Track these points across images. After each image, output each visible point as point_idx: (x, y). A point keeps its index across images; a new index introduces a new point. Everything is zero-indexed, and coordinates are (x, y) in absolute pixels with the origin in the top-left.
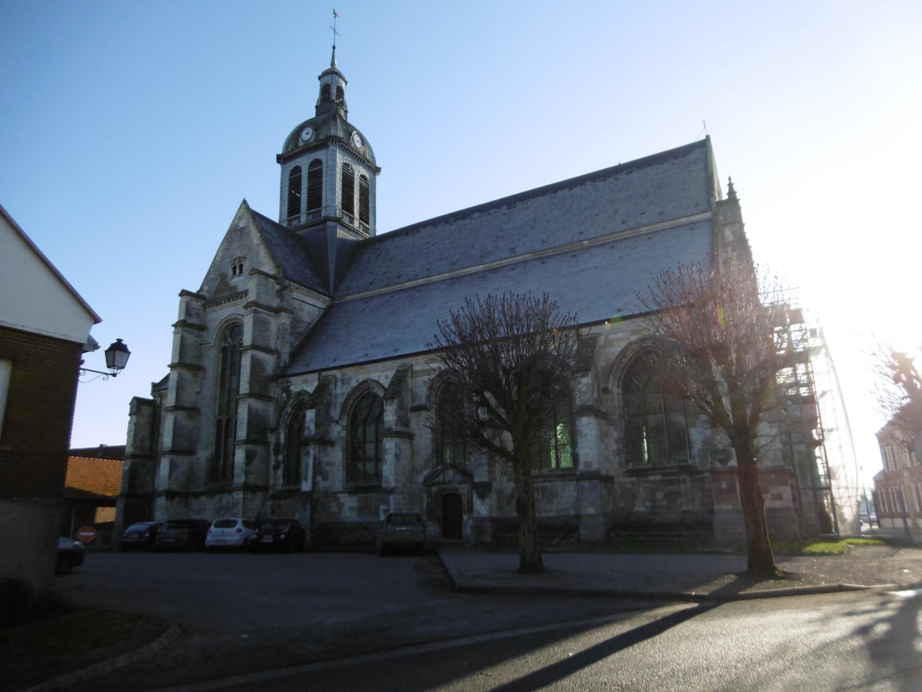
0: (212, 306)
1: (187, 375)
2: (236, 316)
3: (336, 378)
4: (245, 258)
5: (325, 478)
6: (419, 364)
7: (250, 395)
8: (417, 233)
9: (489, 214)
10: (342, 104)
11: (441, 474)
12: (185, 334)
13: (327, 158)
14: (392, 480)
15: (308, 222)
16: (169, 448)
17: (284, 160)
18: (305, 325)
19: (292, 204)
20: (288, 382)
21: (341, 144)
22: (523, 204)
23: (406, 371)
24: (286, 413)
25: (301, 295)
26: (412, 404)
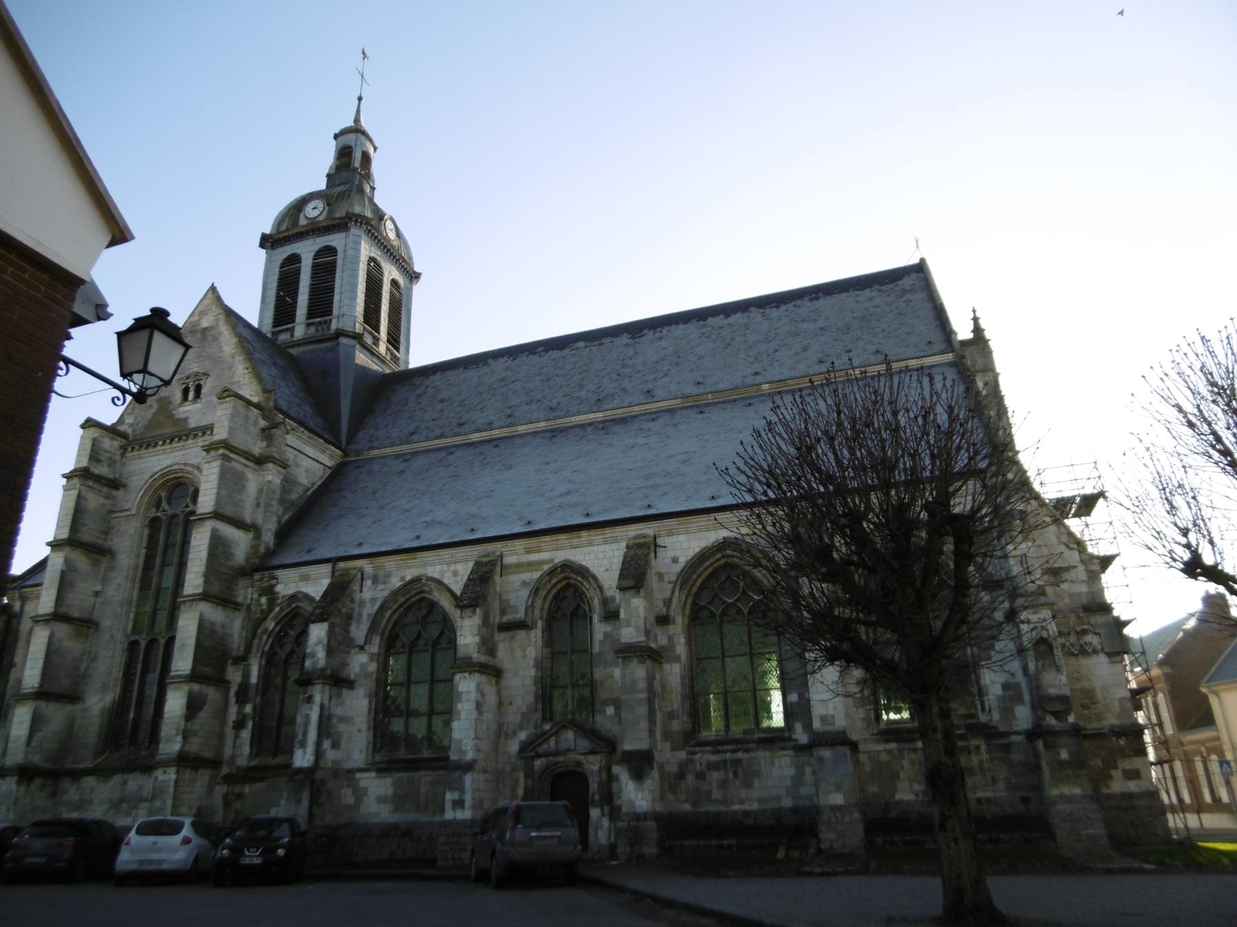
0: (139, 450)
1: (81, 561)
2: (183, 467)
3: (363, 574)
4: (207, 375)
5: (336, 745)
6: (514, 554)
7: (205, 597)
8: (484, 365)
9: (601, 344)
10: (368, 176)
11: (553, 738)
12: (85, 491)
13: (346, 245)
14: (469, 748)
15: (306, 337)
16: (33, 687)
18: (301, 490)
19: (283, 311)
21: (369, 228)
22: (654, 333)
23: (492, 564)
24: (265, 631)
25: (298, 442)
26: (500, 620)
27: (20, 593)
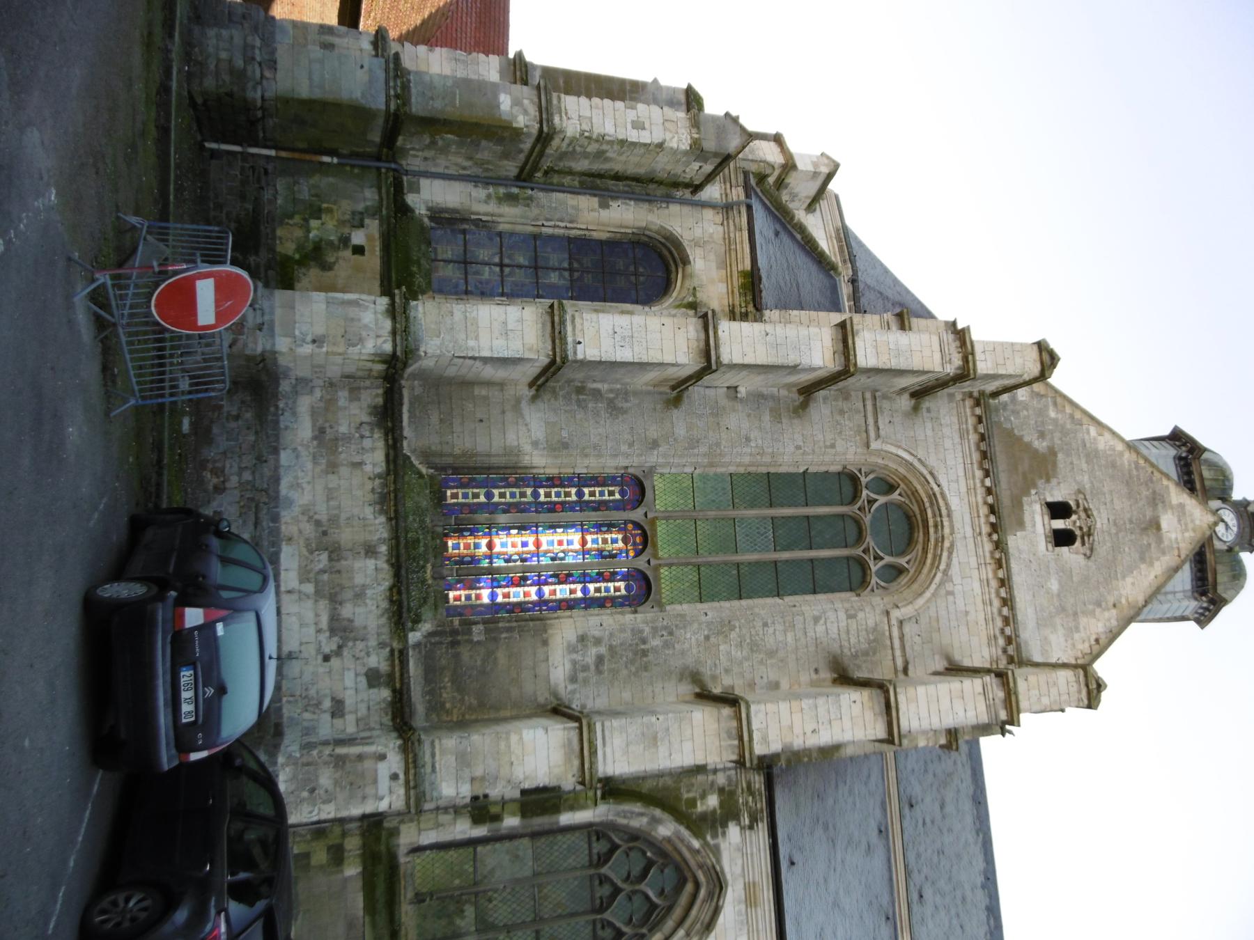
17: (1185, 459)
20: (754, 820)
27: (738, 204)
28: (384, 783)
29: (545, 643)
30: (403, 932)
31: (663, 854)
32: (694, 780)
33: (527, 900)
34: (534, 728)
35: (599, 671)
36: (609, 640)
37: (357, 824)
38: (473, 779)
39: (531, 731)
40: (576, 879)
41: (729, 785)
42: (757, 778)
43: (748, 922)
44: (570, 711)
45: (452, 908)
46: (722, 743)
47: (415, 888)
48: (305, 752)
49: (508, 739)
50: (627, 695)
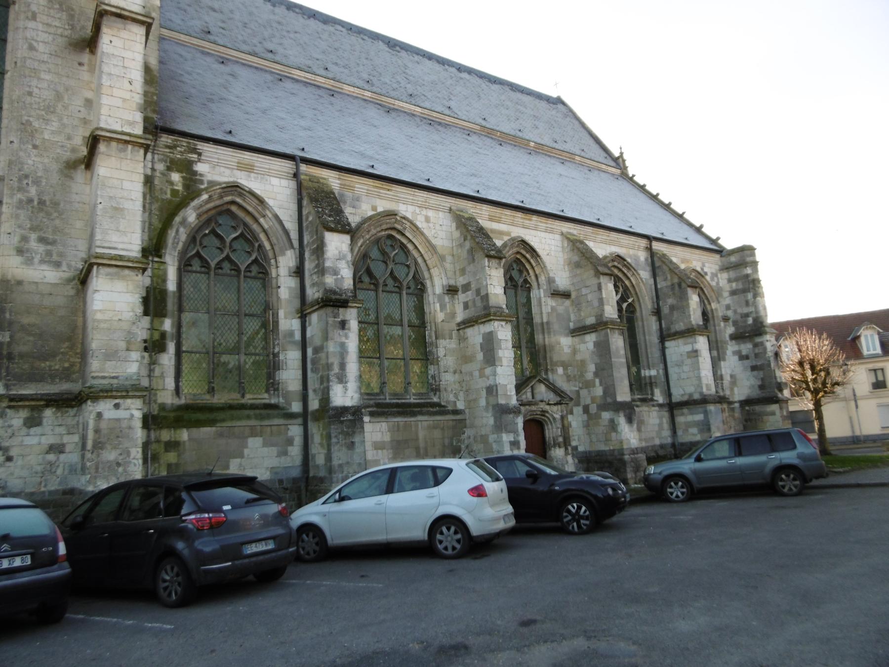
20: (194, 150)
28: (121, 414)
29: (20, 283)
30: (231, 402)
31: (208, 221)
32: (158, 187)
33: (224, 319)
34: (93, 300)
35: (53, 243)
36: (25, 229)
37: (152, 432)
38: (128, 350)
39: (95, 302)
40: (215, 285)
41: (166, 162)
42: (162, 139)
43: (263, 175)
44: (84, 271)
45: (221, 369)
46: (129, 158)
47: (204, 394)
48: (87, 471)
49: (99, 321)
50: (79, 224)
